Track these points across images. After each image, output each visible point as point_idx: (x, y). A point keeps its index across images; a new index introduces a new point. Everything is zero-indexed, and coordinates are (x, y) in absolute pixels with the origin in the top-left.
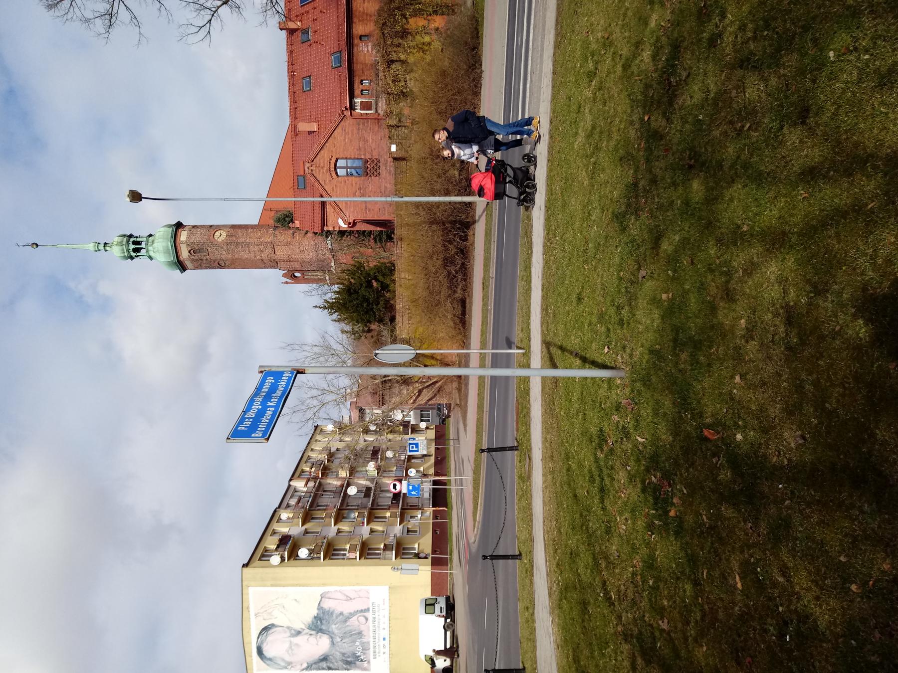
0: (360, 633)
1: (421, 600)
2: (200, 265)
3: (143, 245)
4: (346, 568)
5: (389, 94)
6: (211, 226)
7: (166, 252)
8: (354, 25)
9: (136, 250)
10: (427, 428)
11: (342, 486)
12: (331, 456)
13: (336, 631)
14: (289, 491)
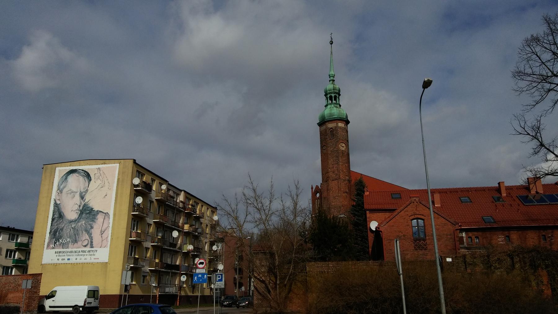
0: (76, 241)
1: (98, 287)
2: (323, 135)
3: (334, 102)
4: (125, 230)
5: (488, 256)
6: (348, 141)
7: (331, 115)
8: (516, 232)
9: (331, 98)
10: (211, 289)
11: (179, 227)
12: (198, 219)
13: (80, 224)
14: (178, 191)
